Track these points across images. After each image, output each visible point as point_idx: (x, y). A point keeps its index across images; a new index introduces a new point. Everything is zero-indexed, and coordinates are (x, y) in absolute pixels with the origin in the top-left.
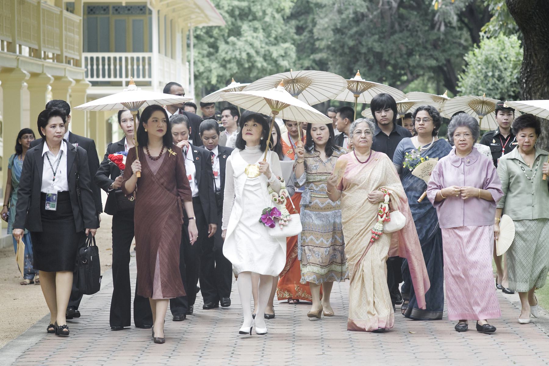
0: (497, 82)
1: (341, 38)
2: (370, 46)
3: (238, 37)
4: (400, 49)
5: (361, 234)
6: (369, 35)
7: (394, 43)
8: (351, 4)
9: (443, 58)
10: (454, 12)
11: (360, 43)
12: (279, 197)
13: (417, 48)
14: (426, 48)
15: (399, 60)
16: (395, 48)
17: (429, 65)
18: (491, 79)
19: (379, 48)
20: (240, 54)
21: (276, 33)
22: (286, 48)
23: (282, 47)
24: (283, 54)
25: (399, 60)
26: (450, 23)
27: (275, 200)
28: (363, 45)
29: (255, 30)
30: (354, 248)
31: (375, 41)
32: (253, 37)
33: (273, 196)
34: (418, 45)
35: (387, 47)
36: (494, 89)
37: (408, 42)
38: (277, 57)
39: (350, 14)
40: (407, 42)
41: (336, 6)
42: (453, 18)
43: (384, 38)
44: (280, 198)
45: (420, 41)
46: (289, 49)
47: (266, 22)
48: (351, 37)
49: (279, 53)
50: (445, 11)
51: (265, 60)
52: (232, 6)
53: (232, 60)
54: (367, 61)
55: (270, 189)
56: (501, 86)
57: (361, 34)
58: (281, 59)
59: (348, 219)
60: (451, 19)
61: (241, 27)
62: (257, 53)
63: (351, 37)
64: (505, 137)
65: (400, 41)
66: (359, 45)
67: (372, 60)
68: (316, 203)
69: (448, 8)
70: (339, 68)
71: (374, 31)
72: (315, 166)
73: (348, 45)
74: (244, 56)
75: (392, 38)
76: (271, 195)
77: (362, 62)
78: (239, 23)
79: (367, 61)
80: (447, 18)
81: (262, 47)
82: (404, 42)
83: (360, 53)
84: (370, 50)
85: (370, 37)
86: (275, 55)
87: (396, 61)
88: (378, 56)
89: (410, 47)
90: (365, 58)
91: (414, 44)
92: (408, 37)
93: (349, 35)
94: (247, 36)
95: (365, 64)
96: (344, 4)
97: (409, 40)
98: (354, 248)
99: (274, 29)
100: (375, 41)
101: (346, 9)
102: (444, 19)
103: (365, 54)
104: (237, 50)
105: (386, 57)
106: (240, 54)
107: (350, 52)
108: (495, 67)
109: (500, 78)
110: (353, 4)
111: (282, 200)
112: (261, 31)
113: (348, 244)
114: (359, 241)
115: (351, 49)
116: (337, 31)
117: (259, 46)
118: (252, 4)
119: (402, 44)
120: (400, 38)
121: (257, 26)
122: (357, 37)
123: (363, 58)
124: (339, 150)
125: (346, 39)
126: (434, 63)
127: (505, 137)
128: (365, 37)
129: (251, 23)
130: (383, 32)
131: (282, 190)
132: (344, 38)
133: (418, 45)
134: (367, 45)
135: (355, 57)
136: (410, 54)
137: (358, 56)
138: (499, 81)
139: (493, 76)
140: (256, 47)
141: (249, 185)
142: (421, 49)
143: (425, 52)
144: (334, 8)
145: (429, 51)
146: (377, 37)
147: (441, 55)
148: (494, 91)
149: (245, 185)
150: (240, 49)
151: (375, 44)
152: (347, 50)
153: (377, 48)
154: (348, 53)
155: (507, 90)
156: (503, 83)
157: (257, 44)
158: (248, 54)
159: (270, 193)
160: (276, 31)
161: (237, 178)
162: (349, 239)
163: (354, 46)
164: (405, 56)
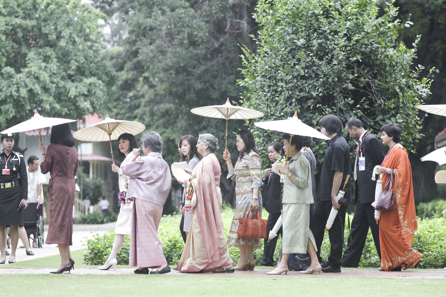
0: (316, 60)
2: (223, 90)
11: (212, 86)
18: (301, 54)
20: (18, 91)
21: (77, 64)
22: (90, 84)
23: (86, 83)
24: (86, 93)
28: (215, 89)
29: (46, 59)
32: (40, 68)
36: (310, 77)
38: (75, 96)
39: (184, 39)
46: (96, 86)
47: (61, 48)
48: (199, 78)
49: (79, 90)
51: (59, 101)
52: (12, 25)
53: (9, 100)
56: (325, 69)
58: (82, 99)
61: (25, 55)
62: (46, 89)
63: (199, 78)
64: (8, 155)
74: (24, 92)
78: (24, 49)
81: (52, 82)
86: (73, 93)
94: (31, 67)
99: (75, 58)
101: (179, 33)
104: (13, 84)
106: (18, 91)
108: (313, 29)
109: (323, 53)
110: (188, 26)
112: (55, 60)
116: (181, 70)
117: (48, 80)
118: (43, 24)
121: (49, 54)
124: (422, 220)
127: (8, 155)
129: (40, 50)
138: (321, 59)
139: (307, 47)
140: (44, 82)
148: (310, 82)
150: (17, 84)
155: (339, 78)
156: (329, 62)
157: (45, 76)
158: (31, 91)
160: (76, 61)
163: (202, 89)
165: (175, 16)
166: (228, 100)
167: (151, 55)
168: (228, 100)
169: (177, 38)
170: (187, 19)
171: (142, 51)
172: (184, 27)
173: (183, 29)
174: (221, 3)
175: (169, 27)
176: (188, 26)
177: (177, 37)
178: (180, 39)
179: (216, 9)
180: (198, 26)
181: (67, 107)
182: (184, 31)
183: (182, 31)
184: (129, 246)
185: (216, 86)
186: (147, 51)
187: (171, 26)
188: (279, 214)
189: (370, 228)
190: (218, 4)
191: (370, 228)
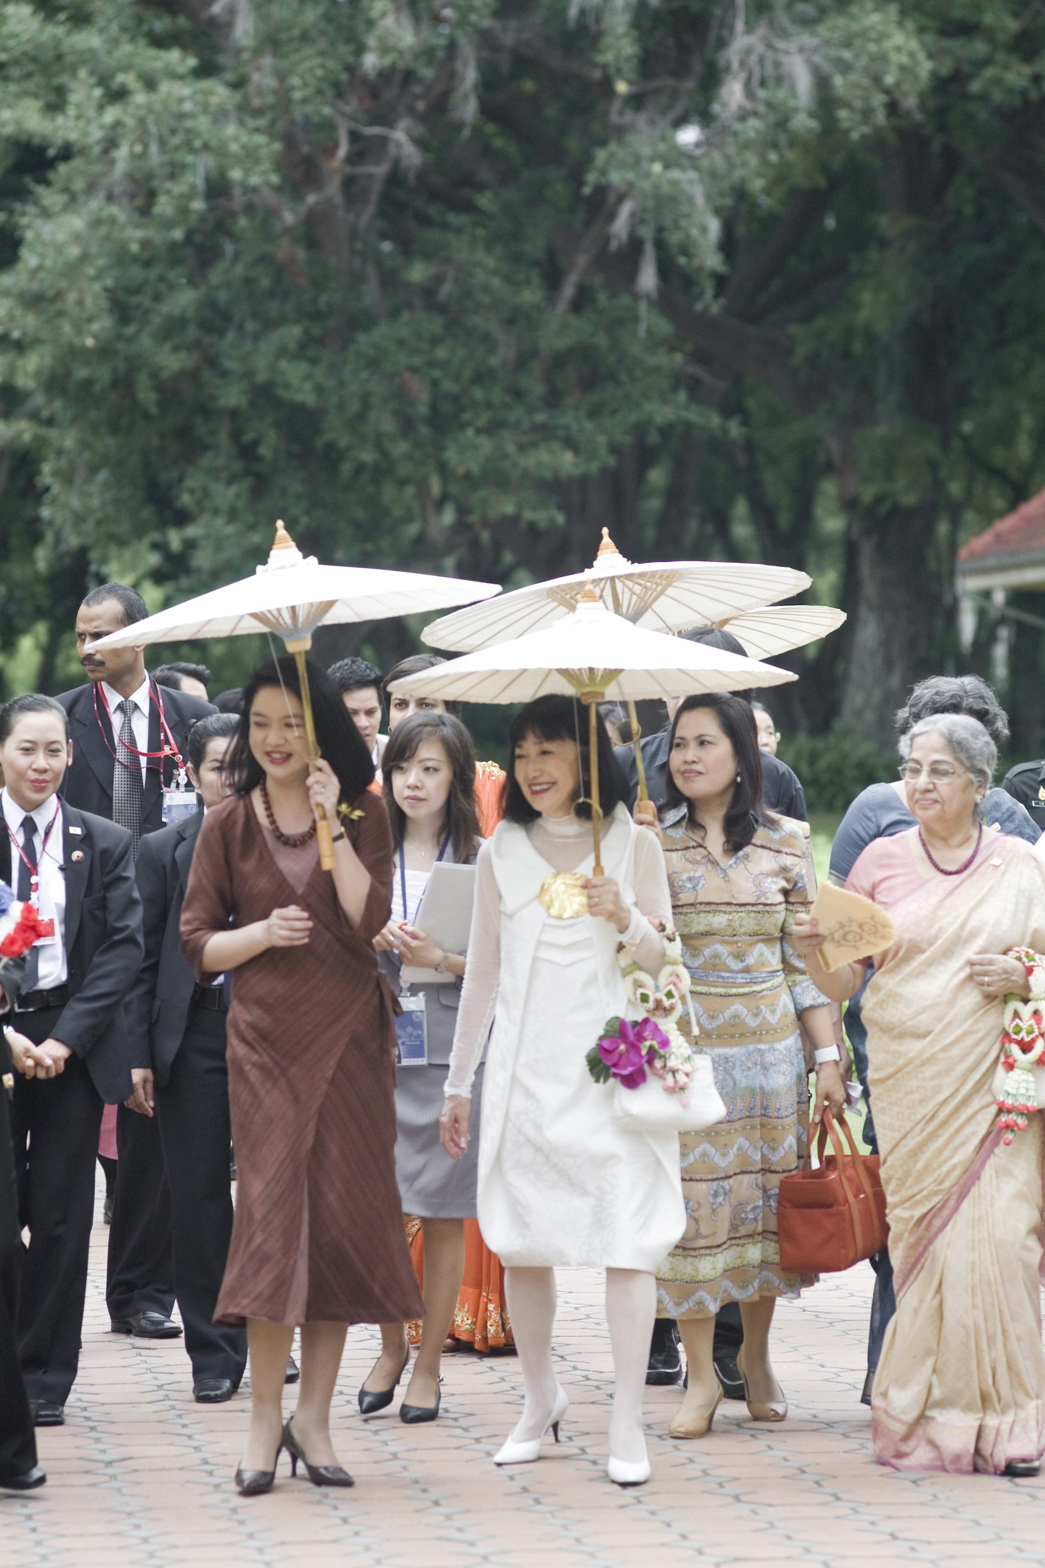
1: (120, 337)
2: (262, 377)
3: (612, 198)
4: (401, 395)
5: (938, 1122)
6: (250, 326)
7: (373, 364)
8: (198, 143)
9: (602, 440)
10: (709, 198)
11: (212, 362)
12: (657, 988)
13: (479, 394)
14: (518, 394)
15: (401, 448)
16: (378, 389)
17: (548, 474)
19: (308, 386)
25: (401, 448)
26: (686, 250)
27: (644, 998)
28: (224, 374)
30: (920, 1165)
31: (282, 352)
33: (638, 984)
34: (482, 377)
35: (342, 384)
37: (444, 365)
39: (191, 195)
40: (431, 364)
41: (122, 153)
42: (704, 230)
43: (320, 342)
44: (661, 996)
45: (494, 361)
48: (171, 329)
50: (666, 189)
54: (247, 452)
55: (624, 960)
57: (215, 319)
59: (891, 1070)
60: (695, 232)
65: (403, 359)
66: (207, 375)
67: (270, 444)
68: (736, 1016)
69: (675, 174)
70: (106, 485)
71: (274, 308)
72: (690, 879)
73: (154, 375)
75: (363, 341)
76: (630, 979)
77: (221, 455)
79: (247, 452)
80: (677, 227)
82: (418, 361)
83: (205, 411)
84: (265, 395)
85: (256, 337)
87: (384, 453)
88: (300, 424)
89: (449, 386)
90: (236, 435)
91: (468, 373)
92: (435, 341)
93: (156, 320)
95: (238, 466)
96: (162, 143)
97: (441, 353)
98: (920, 1165)
100: (282, 352)
101: (175, 170)
102: (660, 230)
103: (234, 414)
105: (335, 432)
107: (163, 404)
110: (206, 147)
111: (667, 1003)
113: (891, 1152)
114: (939, 1142)
115: (168, 391)
119: (413, 370)
120: (401, 343)
122: (192, 332)
123: (223, 438)
125: (146, 342)
126: (567, 462)
128: (231, 336)
130: (316, 316)
131: (667, 970)
132: (130, 340)
133: (482, 377)
134: (248, 374)
135: (184, 433)
136: (445, 419)
137: (201, 429)
141: (551, 945)
142: (497, 396)
143: (517, 414)
144: (112, 162)
145: (532, 410)
146: (293, 333)
147: (588, 425)
149: (540, 944)
151: (283, 364)
152: (147, 396)
153: (300, 384)
154: (154, 410)
159: (625, 973)
161: (511, 916)
162: (897, 1136)
163: (181, 374)
164: (424, 431)
165: (158, 107)
166: (606, 540)
167: (74, 251)
168: (606, 540)
169: (168, 192)
170: (203, 123)
171: (38, 235)
172: (193, 151)
173: (190, 159)
174: (323, 66)
175: (138, 149)
176: (206, 147)
177: (169, 185)
178: (182, 196)
179: (305, 85)
180: (244, 147)
181: (996, 821)
182: (193, 167)
183: (184, 167)
184: (523, 1397)
185: (229, 364)
186: (61, 237)
187: (146, 146)
188: (893, 1310)
189: (176, 1304)
190: (311, 70)
191: (176, 1304)
